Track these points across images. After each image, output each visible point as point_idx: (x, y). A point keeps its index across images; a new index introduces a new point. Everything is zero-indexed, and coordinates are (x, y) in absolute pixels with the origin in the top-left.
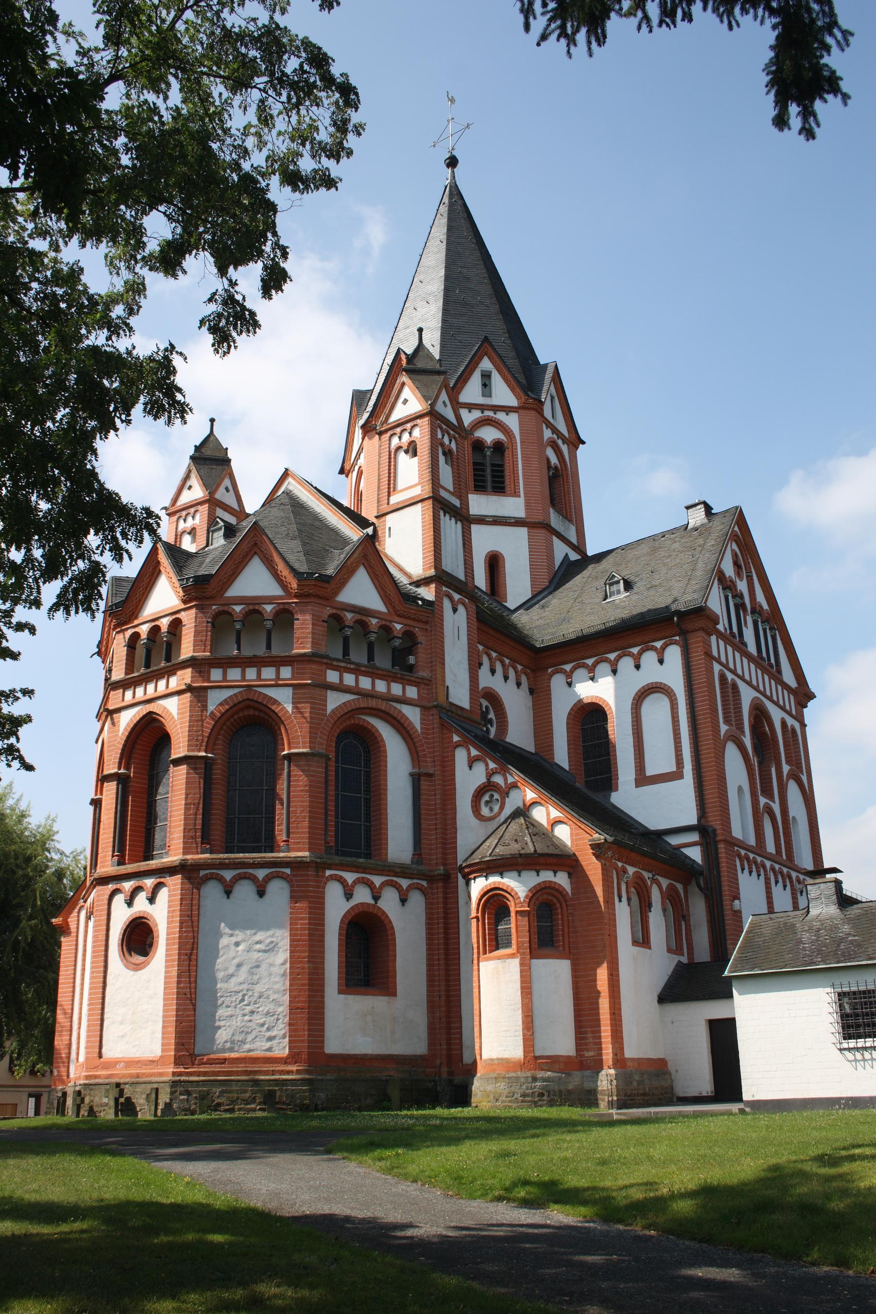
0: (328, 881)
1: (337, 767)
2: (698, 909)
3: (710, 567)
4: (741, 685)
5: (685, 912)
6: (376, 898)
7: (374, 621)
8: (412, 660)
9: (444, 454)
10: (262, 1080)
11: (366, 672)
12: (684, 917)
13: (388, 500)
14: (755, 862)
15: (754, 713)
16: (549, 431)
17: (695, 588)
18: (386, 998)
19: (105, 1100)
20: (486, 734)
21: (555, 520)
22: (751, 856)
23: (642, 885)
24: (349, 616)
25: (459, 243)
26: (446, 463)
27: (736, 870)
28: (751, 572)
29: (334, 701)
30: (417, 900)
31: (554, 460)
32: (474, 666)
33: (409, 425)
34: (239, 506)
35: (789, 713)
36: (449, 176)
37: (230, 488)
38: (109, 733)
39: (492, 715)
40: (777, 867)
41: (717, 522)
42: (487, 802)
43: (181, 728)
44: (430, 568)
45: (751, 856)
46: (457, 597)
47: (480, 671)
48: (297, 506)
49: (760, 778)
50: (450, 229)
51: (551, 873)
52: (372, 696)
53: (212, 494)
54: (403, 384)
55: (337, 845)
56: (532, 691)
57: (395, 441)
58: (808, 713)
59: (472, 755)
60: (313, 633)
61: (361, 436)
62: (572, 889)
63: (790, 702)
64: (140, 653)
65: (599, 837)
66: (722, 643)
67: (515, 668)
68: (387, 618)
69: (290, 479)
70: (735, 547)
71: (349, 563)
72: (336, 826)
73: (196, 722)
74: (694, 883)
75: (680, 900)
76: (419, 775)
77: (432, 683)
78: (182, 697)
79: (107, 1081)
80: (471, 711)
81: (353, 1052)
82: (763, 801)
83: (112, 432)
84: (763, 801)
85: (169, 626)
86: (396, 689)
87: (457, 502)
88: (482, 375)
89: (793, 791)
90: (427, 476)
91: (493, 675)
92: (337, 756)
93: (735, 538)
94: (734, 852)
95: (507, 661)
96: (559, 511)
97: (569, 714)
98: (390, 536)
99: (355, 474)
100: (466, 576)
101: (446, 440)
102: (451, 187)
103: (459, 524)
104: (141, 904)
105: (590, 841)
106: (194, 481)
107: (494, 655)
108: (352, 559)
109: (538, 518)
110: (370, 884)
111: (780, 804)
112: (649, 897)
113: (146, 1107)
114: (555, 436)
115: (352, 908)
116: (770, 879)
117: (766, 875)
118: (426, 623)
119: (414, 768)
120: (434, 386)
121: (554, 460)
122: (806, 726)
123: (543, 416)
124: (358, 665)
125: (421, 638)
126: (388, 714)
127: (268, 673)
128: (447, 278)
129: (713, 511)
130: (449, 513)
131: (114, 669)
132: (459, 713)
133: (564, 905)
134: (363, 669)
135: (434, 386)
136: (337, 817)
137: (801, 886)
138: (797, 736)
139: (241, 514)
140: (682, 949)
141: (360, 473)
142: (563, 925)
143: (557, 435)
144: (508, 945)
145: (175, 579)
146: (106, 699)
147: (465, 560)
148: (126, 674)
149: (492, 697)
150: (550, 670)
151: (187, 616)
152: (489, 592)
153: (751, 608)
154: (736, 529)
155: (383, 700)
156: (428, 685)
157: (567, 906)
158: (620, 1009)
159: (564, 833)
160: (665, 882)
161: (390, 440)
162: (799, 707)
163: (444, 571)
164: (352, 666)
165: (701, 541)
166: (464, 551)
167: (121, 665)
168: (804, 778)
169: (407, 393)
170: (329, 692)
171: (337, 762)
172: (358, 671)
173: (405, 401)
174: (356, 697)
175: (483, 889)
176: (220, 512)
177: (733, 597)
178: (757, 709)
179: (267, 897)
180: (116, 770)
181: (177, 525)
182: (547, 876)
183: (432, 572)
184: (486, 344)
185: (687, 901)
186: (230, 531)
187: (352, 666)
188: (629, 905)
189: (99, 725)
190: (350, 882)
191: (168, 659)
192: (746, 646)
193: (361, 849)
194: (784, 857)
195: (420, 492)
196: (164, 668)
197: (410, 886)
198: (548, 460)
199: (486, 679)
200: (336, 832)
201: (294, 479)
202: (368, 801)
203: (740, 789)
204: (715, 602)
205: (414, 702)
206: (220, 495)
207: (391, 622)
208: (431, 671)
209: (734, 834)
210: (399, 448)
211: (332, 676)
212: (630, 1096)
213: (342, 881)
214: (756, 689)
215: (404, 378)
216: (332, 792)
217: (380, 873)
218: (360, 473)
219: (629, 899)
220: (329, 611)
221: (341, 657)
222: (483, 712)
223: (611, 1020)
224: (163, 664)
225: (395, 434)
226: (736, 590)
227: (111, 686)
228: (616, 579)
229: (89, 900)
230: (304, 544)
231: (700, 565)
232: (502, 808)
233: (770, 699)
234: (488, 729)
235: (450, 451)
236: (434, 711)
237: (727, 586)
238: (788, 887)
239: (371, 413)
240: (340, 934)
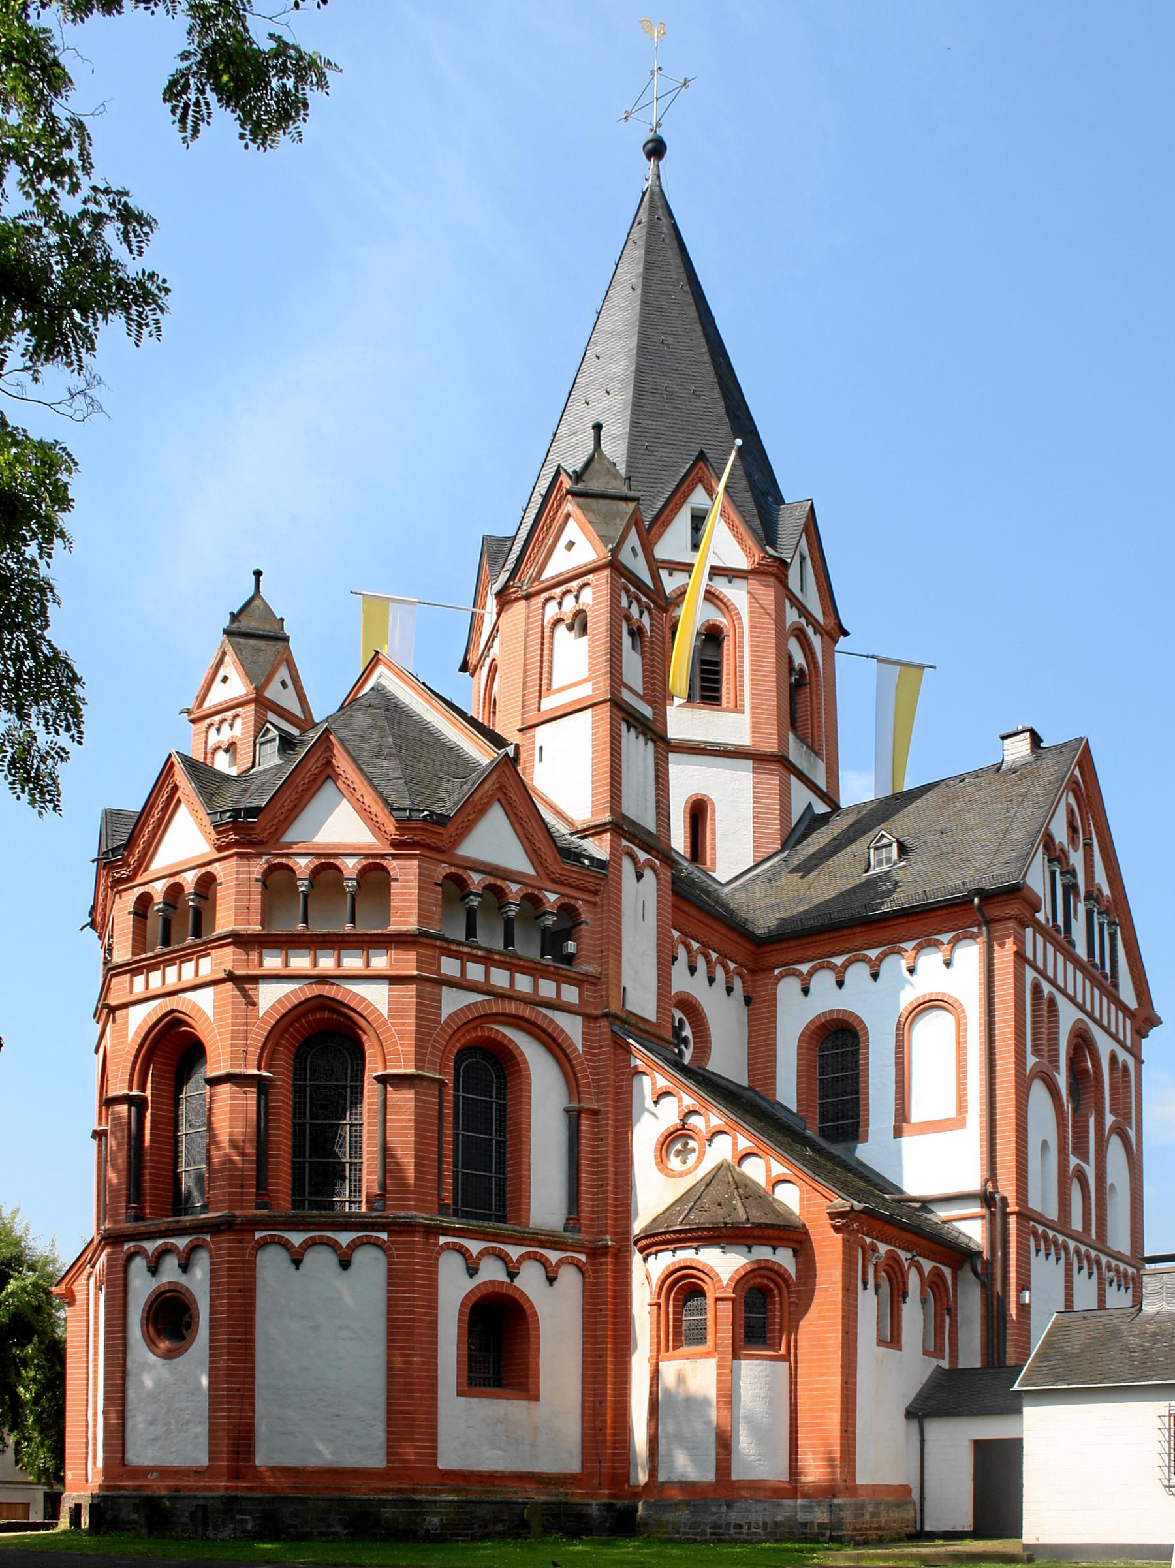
0: (779, 980)
1: (456, 1097)
2: (971, 1303)
3: (1034, 826)
4: (1061, 1000)
5: (951, 1304)
6: (512, 1275)
7: (515, 887)
8: (571, 947)
9: (631, 633)
10: (350, 1500)
11: (501, 962)
12: (949, 1310)
13: (539, 703)
14: (1055, 1243)
15: (1075, 1041)
16: (795, 612)
17: (1009, 856)
18: (525, 1403)
19: (135, 1517)
20: (678, 1058)
21: (796, 753)
22: (1051, 1233)
23: (897, 1269)
24: (476, 878)
25: (662, 292)
26: (634, 648)
27: (1029, 1252)
28: (1091, 839)
29: (452, 1002)
30: (570, 1279)
31: (799, 659)
32: (665, 961)
33: (575, 584)
34: (304, 713)
35: (1122, 1044)
36: (651, 174)
37: (289, 682)
38: (112, 1038)
39: (687, 1032)
40: (1083, 1248)
41: (1048, 758)
42: (678, 1153)
43: (220, 1034)
44: (603, 810)
45: (1051, 1233)
46: (643, 856)
47: (673, 968)
48: (391, 710)
49: (1074, 1132)
50: (649, 266)
51: (769, 1250)
52: (511, 998)
53: (259, 690)
54: (568, 516)
55: (456, 1203)
56: (748, 1001)
57: (552, 610)
58: (1150, 1045)
59: (659, 1086)
60: (420, 901)
61: (495, 610)
62: (798, 1271)
63: (1125, 1029)
64: (155, 924)
65: (841, 1203)
66: (1040, 940)
67: (725, 966)
68: (537, 884)
69: (381, 669)
70: (1072, 800)
71: (477, 797)
72: (456, 1178)
73: (243, 1026)
74: (968, 1267)
75: (946, 1290)
76: (579, 1112)
77: (600, 983)
78: (220, 987)
79: (134, 1493)
80: (658, 1025)
81: (476, 1468)
82: (1073, 1161)
83: (58, 542)
84: (1073, 1161)
85: (197, 884)
86: (547, 989)
87: (647, 711)
88: (692, 517)
89: (1115, 1151)
90: (604, 667)
91: (692, 974)
92: (456, 1081)
93: (1074, 788)
94: (1027, 1227)
95: (714, 956)
96: (802, 739)
97: (803, 1034)
98: (541, 760)
99: (484, 671)
100: (658, 826)
101: (635, 611)
102: (652, 193)
103: (651, 745)
104: (170, 1272)
105: (829, 1207)
106: (230, 668)
107: (695, 945)
108: (480, 793)
109: (770, 745)
110: (503, 1258)
111: (1096, 1166)
112: (905, 1284)
113: (190, 1526)
114: (803, 621)
115: (478, 1287)
116: (1071, 1264)
117: (1067, 1259)
118: (595, 893)
119: (571, 1100)
120: (618, 521)
121: (799, 659)
122: (1143, 1062)
123: (786, 586)
124: (489, 951)
125: (586, 915)
126: (534, 1024)
127: (353, 962)
128: (643, 350)
129: (1042, 745)
130: (636, 728)
131: (115, 947)
132: (641, 1025)
133: (785, 1290)
134: (497, 957)
135: (618, 521)
136: (456, 1166)
137: (1112, 1274)
138: (1129, 1076)
139: (307, 723)
140: (942, 1351)
141: (493, 670)
142: (781, 1317)
143: (806, 618)
144: (702, 1340)
145: (202, 813)
146: (105, 989)
147: (658, 801)
148: (134, 954)
149: (689, 1006)
150: (777, 972)
151: (223, 869)
152: (688, 855)
153: (1086, 892)
154: (1077, 772)
155: (526, 1003)
156: (595, 984)
157: (789, 1293)
158: (854, 1426)
159: (789, 1197)
160: (927, 1265)
161: (543, 608)
162: (1136, 1036)
163: (624, 817)
164: (480, 953)
165: (1021, 789)
166: (657, 788)
167: (125, 941)
168: (1132, 1133)
169: (572, 531)
170: (444, 988)
171: (456, 1089)
172: (488, 960)
173: (570, 545)
174: (487, 998)
175: (668, 1267)
176: (271, 717)
177: (1062, 874)
178: (1078, 1036)
179: (353, 1267)
180: (126, 1091)
181: (207, 737)
182: (763, 1253)
183: (607, 817)
184: (701, 464)
185: (955, 1290)
186: (287, 744)
187: (480, 953)
188: (877, 1293)
189: (98, 1028)
190: (475, 1254)
191: (197, 933)
192: (1074, 947)
193: (490, 1209)
194: (1094, 1237)
195: (590, 692)
196: (190, 947)
197: (561, 1260)
198: (790, 660)
199: (682, 981)
200: (455, 1185)
201: (389, 668)
202: (501, 1145)
203: (1045, 1145)
204: (1037, 879)
205: (573, 1008)
206: (273, 692)
207: (540, 889)
208: (601, 965)
209: (1031, 1205)
210: (559, 621)
211: (450, 967)
212: (860, 1530)
213: (463, 1252)
214: (1081, 1008)
215: (569, 506)
216: (449, 1130)
217: (518, 1241)
218: (493, 670)
219: (877, 1287)
220: (444, 869)
221: (463, 939)
222: (674, 1027)
223: (842, 1438)
224: (189, 940)
225: (552, 598)
226: (1068, 863)
227: (112, 971)
228: (885, 841)
229: (97, 1265)
230: (405, 766)
231: (1018, 824)
232: (700, 1160)
233: (1099, 1023)
234: (681, 1052)
235: (640, 629)
236: (603, 1023)
237: (1056, 856)
238: (1095, 1276)
239: (510, 570)
240: (459, 1321)
